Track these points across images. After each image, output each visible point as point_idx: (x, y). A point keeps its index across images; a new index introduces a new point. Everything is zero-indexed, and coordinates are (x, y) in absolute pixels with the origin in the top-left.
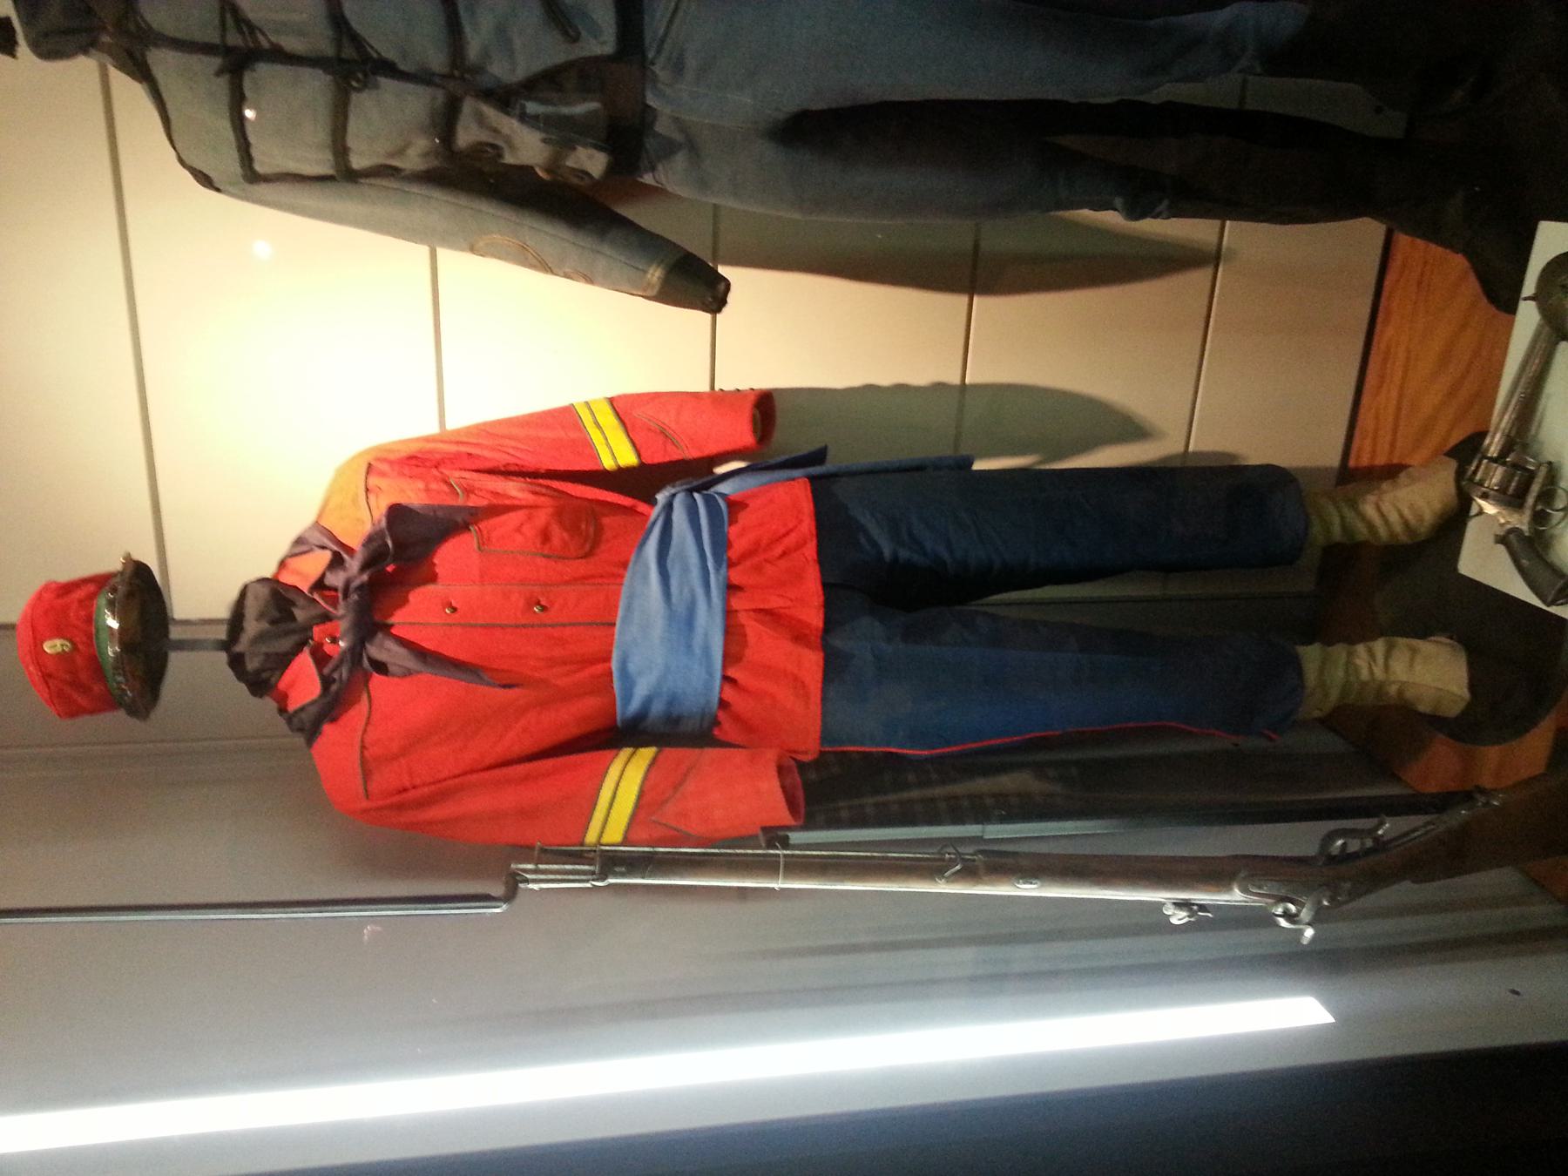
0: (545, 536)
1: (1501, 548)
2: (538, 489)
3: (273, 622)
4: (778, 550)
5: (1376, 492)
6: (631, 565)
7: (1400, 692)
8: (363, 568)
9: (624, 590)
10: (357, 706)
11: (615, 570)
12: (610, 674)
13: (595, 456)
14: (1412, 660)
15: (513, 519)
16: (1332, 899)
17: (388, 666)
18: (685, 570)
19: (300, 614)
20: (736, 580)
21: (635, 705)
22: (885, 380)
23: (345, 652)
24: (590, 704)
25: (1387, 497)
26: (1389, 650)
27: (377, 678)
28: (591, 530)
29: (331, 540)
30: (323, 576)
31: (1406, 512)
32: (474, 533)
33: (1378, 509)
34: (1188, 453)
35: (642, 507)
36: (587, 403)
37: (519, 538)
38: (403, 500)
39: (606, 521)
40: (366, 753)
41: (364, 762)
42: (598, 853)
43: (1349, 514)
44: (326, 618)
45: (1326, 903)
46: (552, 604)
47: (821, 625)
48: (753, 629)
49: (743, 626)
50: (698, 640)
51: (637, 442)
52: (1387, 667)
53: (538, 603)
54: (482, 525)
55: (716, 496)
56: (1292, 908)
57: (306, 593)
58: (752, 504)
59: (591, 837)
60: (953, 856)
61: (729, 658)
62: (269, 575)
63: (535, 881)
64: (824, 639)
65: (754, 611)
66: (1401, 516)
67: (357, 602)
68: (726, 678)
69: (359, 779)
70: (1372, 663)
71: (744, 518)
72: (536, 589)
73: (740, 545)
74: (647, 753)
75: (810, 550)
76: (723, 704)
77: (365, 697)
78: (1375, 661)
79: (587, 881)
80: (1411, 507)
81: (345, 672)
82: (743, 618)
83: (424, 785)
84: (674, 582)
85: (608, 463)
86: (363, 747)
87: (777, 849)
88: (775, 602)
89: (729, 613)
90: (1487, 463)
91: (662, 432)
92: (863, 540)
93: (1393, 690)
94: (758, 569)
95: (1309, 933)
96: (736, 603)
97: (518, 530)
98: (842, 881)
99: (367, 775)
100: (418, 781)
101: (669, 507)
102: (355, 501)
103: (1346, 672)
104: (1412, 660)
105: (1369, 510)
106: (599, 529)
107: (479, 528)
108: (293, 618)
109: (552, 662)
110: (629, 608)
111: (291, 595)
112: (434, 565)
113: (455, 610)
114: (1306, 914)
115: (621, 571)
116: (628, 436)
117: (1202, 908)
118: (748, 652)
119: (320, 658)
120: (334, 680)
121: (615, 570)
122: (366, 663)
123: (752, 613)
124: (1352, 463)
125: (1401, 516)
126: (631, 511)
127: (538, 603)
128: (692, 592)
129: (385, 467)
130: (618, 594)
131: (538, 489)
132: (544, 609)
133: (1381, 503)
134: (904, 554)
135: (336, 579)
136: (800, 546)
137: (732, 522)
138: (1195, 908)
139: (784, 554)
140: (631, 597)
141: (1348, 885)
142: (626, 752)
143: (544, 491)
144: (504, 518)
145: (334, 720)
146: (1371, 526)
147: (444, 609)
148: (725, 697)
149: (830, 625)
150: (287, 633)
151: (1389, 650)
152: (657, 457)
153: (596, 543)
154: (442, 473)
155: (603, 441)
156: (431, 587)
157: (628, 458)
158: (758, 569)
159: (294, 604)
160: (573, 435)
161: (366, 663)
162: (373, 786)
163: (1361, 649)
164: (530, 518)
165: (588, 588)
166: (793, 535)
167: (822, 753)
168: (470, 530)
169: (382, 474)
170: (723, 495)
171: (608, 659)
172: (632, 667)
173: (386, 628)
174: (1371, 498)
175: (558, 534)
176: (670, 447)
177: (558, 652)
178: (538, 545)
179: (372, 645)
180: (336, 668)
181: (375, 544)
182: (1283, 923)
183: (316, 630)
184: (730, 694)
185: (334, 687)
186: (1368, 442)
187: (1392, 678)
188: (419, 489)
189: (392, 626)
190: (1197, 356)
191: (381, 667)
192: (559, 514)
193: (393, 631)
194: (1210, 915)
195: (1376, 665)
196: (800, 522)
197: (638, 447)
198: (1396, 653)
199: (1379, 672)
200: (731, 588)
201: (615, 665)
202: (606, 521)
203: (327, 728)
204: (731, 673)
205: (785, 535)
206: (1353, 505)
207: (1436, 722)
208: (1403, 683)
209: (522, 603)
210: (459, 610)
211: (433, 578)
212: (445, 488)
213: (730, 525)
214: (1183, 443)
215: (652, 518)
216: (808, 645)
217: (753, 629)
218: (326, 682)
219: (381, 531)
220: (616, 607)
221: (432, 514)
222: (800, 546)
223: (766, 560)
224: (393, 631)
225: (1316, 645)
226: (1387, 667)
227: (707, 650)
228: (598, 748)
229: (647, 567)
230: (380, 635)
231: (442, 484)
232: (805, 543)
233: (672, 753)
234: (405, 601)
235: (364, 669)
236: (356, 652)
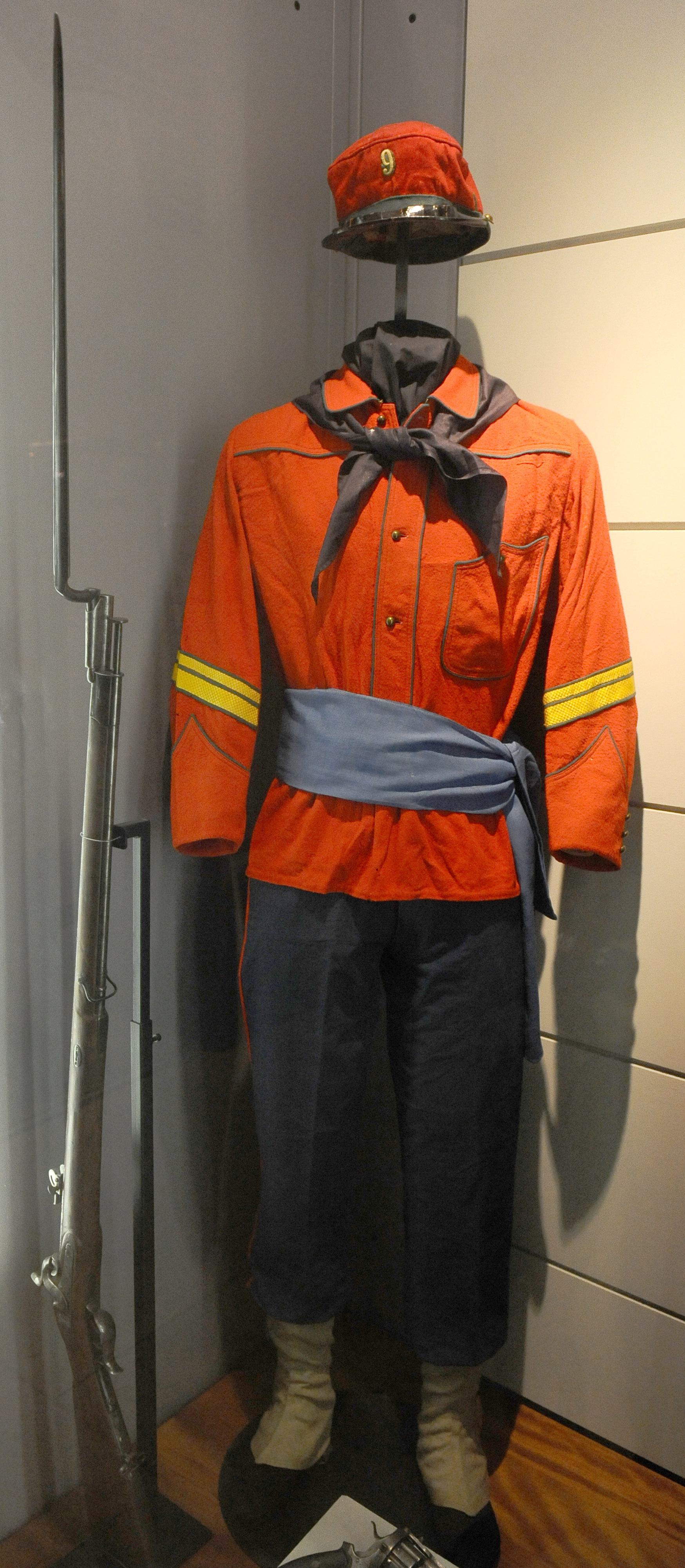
0: (467, 631)
1: (337, 1546)
2: (527, 625)
3: (400, 364)
4: (433, 862)
5: (464, 1431)
6: (432, 714)
7: (279, 1401)
8: (441, 452)
9: (405, 706)
10: (320, 445)
11: (425, 699)
12: (327, 688)
13: (557, 686)
14: (305, 1421)
15: (490, 600)
16: (55, 1308)
17: (347, 476)
18: (423, 768)
19: (408, 391)
20: (405, 817)
21: (299, 706)
22: (642, 982)
23: (364, 434)
24: (303, 666)
25: (456, 1440)
26: (320, 1404)
27: (338, 462)
28: (473, 677)
29: (493, 416)
30: (447, 411)
31: (436, 1455)
32: (477, 559)
33: (446, 1430)
34: (546, 1262)
35: (500, 728)
36: (632, 674)
37: (466, 605)
38: (510, 488)
39: (485, 691)
40: (272, 455)
41: (267, 452)
42: (112, 674)
43: (445, 1401)
44: (402, 415)
45: (54, 1303)
46: (393, 634)
47: (354, 895)
48: (358, 827)
49: (360, 819)
50: (349, 774)
51: (570, 728)
52: (298, 1396)
53: (396, 621)
54: (485, 568)
55: (505, 804)
56: (54, 1274)
57: (431, 396)
58: (494, 840)
59: (184, 659)
60: (101, 995)
61: (332, 804)
62: (463, 353)
63: (90, 615)
64: (342, 895)
65: (373, 832)
66: (435, 1449)
67: (407, 445)
68: (314, 797)
69: (248, 450)
70: (304, 1385)
71: (473, 832)
72: (412, 620)
73: (443, 825)
74: (252, 716)
75: (430, 893)
76: (293, 791)
77: (327, 453)
78: (308, 1388)
79: (89, 664)
80: (441, 1460)
81: (349, 434)
82: (366, 820)
83: (241, 508)
84: (407, 756)
85: (550, 696)
86: (279, 452)
87: (112, 837)
88: (377, 855)
89: (372, 808)
90: (415, 1560)
91: (579, 753)
92: (441, 945)
93: (281, 1395)
94: (414, 841)
95: (37, 1281)
96: (380, 815)
97: (476, 603)
98: (83, 893)
99: (255, 455)
100: (245, 502)
101: (498, 755)
102: (529, 441)
103: (297, 1361)
104: (305, 1421)
105: (445, 1421)
106: (474, 685)
107: (481, 565)
108: (404, 383)
109: (338, 631)
110: (385, 709)
111: (430, 380)
112: (446, 521)
113: (396, 539)
114: (49, 1283)
115: (424, 703)
116: (579, 719)
117: (59, 1198)
118: (334, 821)
119: (364, 411)
120: (340, 424)
121: (425, 699)
122: (354, 453)
123: (370, 829)
124: (524, 1408)
125: (435, 1449)
126: (500, 717)
127: (396, 621)
128: (394, 774)
129: (564, 471)
130: (401, 700)
131: (527, 625)
132: (390, 627)
133: (449, 1434)
134: (423, 983)
135: (442, 424)
136: (436, 882)
137: (471, 818)
138: (59, 1192)
139: (429, 866)
140: (396, 713)
141: (68, 1324)
142: (256, 697)
143: (525, 631)
144: (492, 591)
145: (310, 423)
146: (431, 1418)
147: (398, 529)
148: (298, 793)
149: (355, 903)
150: (389, 378)
151: (320, 1404)
152: (553, 747)
153: (461, 682)
154: (554, 527)
155: (576, 692)
156: (422, 516)
157: (554, 717)
158: (414, 841)
159: (420, 384)
160: (587, 662)
161: (354, 453)
162: (243, 462)
163: (325, 1377)
164: (488, 616)
165: (409, 671)
166: (449, 877)
167: (247, 878)
168: (479, 556)
169: (555, 470)
170: (505, 812)
171: (341, 686)
172: (330, 708)
173: (384, 474)
174: (457, 1425)
175: (469, 643)
176: (560, 761)
177: (347, 639)
178: (456, 624)
179: (370, 458)
180: (351, 426)
181: (464, 463)
182: (46, 1263)
183: (392, 406)
184: (299, 799)
185: (334, 424)
186: (538, 1430)
187: (289, 1398)
188: (535, 506)
189: (387, 478)
190: (632, 1293)
191: (346, 470)
192: (491, 644)
193: (383, 480)
194: (55, 1203)
195: (303, 1387)
196: (461, 886)
197: (565, 729)
198: (312, 1407)
199: (295, 1388)
200: (396, 812)
201: (333, 691)
202: (485, 691)
203: (303, 418)
204: (318, 803)
205: (450, 870)
206: (449, 1409)
207: (252, 1428)
208: (284, 1406)
209: (396, 605)
210: (394, 543)
211: (432, 518)
212: (534, 531)
213: (468, 815)
214: (553, 1259)
215: (486, 738)
216: (333, 881)
217: (358, 827)
218: (339, 417)
219: (474, 467)
220: (388, 698)
221: (494, 519)
222: (436, 882)
223: (423, 848)
224: (383, 480)
225: (332, 1338)
226: (298, 1396)
227: (338, 782)
228: (265, 671)
229: (427, 729)
230: (379, 467)
231: (539, 528)
232: (438, 889)
233: (249, 741)
234: (410, 492)
235: (349, 452)
236: (364, 445)
